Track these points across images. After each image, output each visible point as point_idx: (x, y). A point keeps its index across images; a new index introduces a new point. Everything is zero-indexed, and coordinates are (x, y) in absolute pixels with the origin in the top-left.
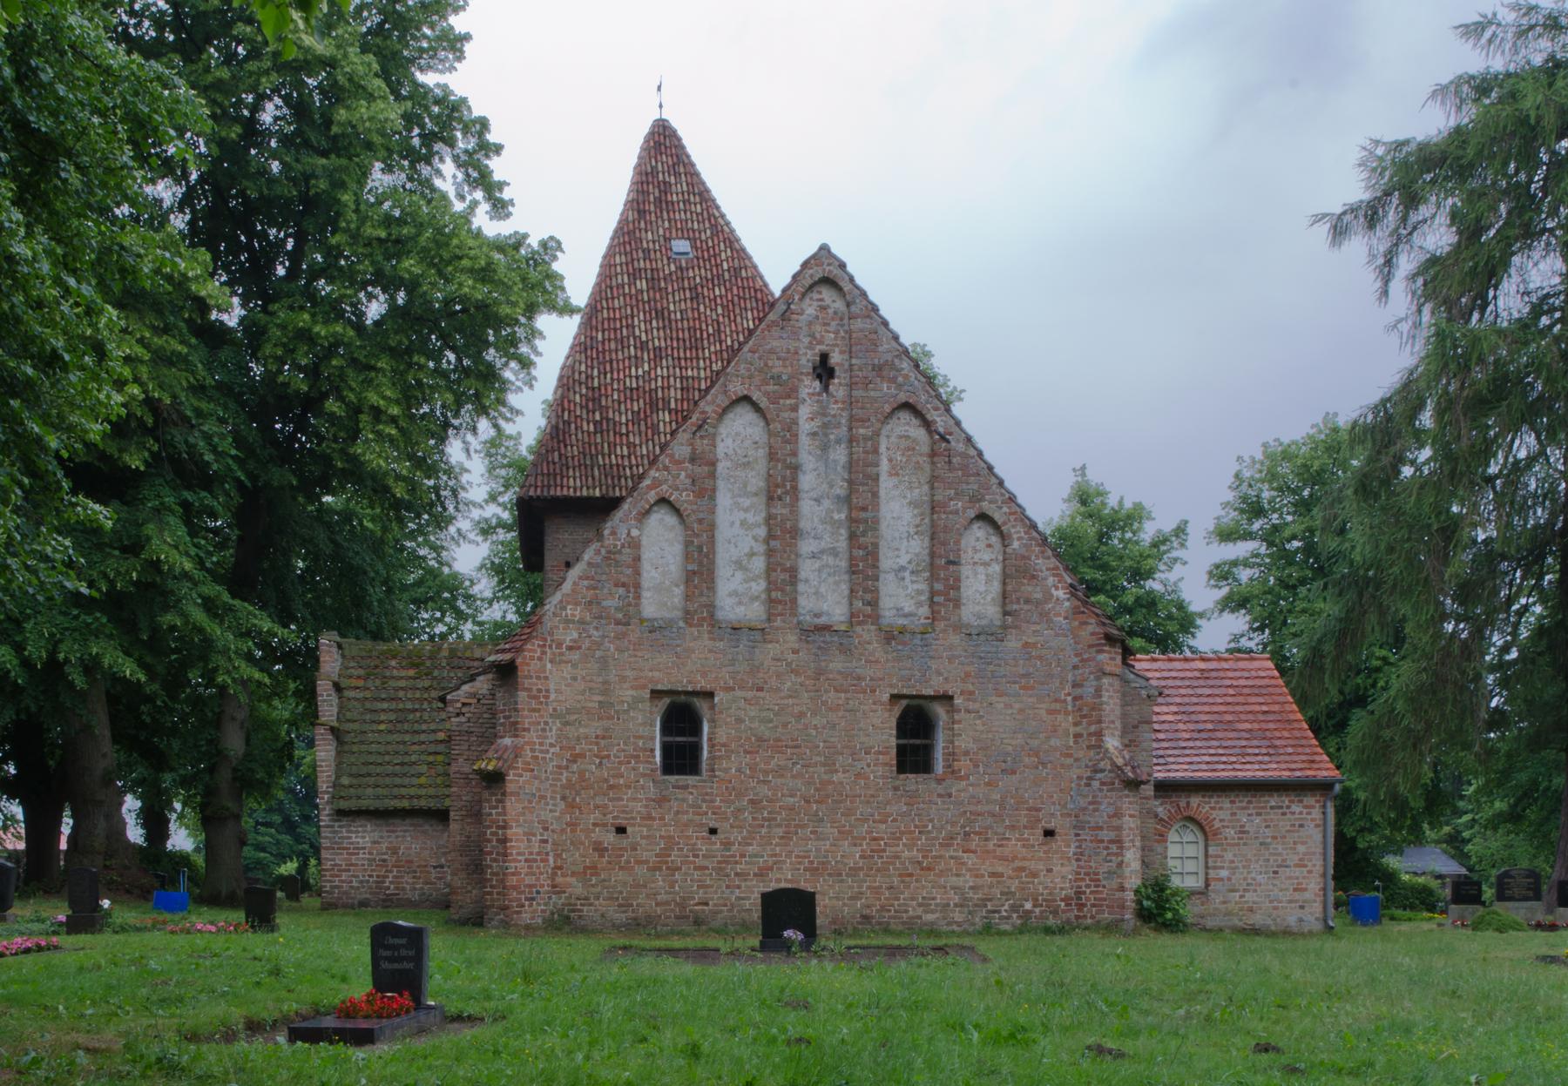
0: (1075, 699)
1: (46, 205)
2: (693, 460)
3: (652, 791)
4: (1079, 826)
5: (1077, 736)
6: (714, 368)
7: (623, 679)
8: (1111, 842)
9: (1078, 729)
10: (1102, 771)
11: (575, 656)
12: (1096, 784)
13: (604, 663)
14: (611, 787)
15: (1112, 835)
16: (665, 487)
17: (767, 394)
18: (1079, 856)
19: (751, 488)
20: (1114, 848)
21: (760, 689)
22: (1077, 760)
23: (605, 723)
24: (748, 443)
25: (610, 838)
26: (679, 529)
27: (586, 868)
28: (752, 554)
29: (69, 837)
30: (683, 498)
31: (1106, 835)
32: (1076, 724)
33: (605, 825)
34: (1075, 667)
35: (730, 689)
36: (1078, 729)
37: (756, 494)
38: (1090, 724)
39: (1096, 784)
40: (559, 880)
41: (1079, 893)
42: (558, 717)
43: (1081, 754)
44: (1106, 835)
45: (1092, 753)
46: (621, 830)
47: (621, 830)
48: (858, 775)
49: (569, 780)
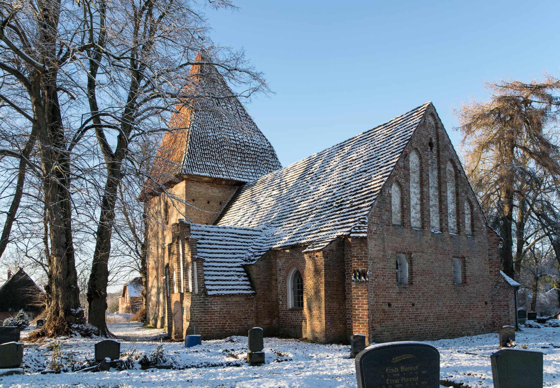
0: (489, 260)
1: (130, 69)
2: (404, 168)
3: (397, 290)
4: (493, 301)
5: (491, 271)
6: (21, 148)
7: (388, 246)
8: (505, 305)
9: (491, 269)
10: (501, 283)
11: (376, 237)
12: (498, 287)
13: (383, 239)
14: (387, 288)
15: (505, 303)
16: (397, 176)
17: (421, 149)
18: (493, 310)
19: (416, 181)
20: (506, 307)
21: (423, 252)
22: (491, 279)
23: (385, 263)
24: (414, 165)
25: (387, 308)
26: (399, 192)
27: (381, 320)
28: (417, 204)
29: (173, 285)
30: (402, 181)
31: (503, 303)
32: (490, 268)
33: (385, 302)
34: (489, 250)
35: (416, 252)
36: (491, 269)
37: (417, 183)
38: (495, 267)
39: (498, 287)
40: (374, 325)
41: (494, 322)
42: (371, 260)
43: (492, 277)
44: (503, 303)
45: (496, 277)
46: (390, 305)
47: (390, 305)
48: (446, 284)
49: (375, 285)
